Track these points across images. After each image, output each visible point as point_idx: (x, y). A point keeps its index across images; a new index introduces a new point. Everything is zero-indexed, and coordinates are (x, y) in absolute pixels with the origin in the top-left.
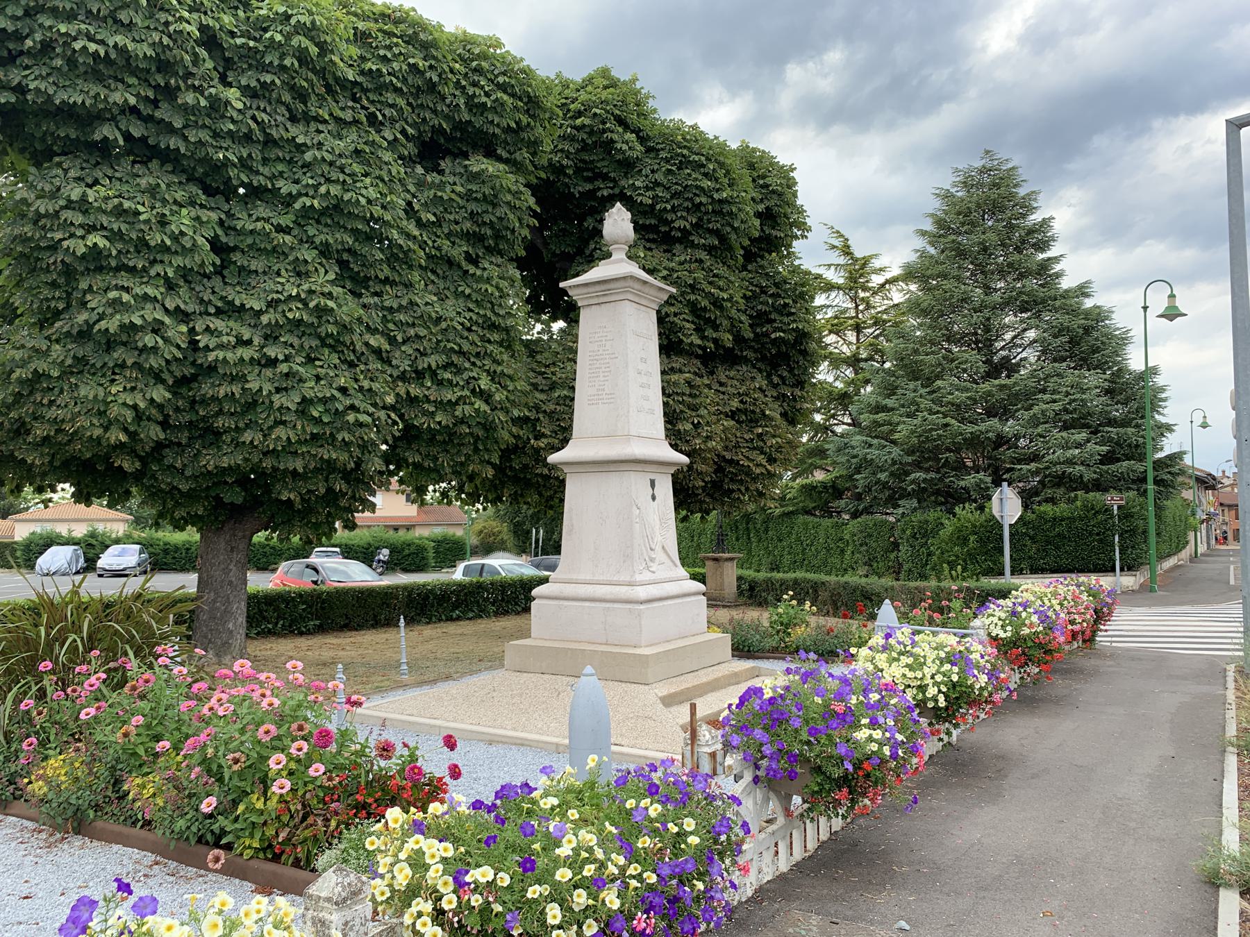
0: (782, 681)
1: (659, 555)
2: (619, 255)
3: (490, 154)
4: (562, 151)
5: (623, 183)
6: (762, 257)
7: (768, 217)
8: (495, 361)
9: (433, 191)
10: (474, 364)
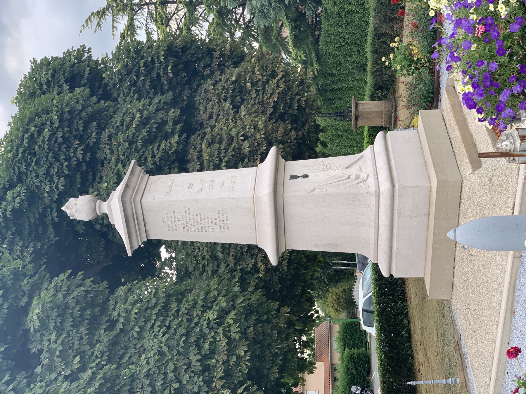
0: (457, 75)
1: (354, 171)
2: (104, 207)
3: (25, 310)
4: (22, 252)
5: (47, 201)
6: (107, 85)
7: (73, 81)
8: (194, 305)
9: (55, 358)
10: (197, 324)
